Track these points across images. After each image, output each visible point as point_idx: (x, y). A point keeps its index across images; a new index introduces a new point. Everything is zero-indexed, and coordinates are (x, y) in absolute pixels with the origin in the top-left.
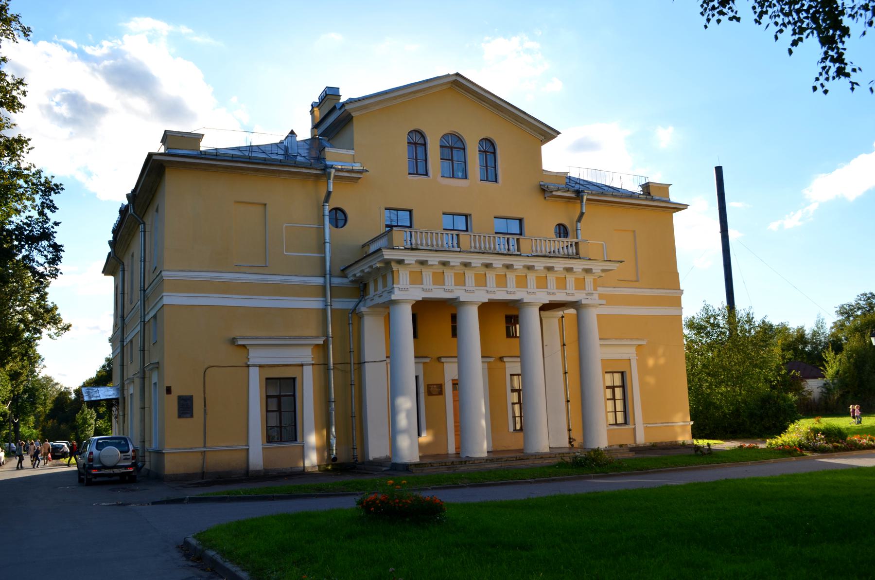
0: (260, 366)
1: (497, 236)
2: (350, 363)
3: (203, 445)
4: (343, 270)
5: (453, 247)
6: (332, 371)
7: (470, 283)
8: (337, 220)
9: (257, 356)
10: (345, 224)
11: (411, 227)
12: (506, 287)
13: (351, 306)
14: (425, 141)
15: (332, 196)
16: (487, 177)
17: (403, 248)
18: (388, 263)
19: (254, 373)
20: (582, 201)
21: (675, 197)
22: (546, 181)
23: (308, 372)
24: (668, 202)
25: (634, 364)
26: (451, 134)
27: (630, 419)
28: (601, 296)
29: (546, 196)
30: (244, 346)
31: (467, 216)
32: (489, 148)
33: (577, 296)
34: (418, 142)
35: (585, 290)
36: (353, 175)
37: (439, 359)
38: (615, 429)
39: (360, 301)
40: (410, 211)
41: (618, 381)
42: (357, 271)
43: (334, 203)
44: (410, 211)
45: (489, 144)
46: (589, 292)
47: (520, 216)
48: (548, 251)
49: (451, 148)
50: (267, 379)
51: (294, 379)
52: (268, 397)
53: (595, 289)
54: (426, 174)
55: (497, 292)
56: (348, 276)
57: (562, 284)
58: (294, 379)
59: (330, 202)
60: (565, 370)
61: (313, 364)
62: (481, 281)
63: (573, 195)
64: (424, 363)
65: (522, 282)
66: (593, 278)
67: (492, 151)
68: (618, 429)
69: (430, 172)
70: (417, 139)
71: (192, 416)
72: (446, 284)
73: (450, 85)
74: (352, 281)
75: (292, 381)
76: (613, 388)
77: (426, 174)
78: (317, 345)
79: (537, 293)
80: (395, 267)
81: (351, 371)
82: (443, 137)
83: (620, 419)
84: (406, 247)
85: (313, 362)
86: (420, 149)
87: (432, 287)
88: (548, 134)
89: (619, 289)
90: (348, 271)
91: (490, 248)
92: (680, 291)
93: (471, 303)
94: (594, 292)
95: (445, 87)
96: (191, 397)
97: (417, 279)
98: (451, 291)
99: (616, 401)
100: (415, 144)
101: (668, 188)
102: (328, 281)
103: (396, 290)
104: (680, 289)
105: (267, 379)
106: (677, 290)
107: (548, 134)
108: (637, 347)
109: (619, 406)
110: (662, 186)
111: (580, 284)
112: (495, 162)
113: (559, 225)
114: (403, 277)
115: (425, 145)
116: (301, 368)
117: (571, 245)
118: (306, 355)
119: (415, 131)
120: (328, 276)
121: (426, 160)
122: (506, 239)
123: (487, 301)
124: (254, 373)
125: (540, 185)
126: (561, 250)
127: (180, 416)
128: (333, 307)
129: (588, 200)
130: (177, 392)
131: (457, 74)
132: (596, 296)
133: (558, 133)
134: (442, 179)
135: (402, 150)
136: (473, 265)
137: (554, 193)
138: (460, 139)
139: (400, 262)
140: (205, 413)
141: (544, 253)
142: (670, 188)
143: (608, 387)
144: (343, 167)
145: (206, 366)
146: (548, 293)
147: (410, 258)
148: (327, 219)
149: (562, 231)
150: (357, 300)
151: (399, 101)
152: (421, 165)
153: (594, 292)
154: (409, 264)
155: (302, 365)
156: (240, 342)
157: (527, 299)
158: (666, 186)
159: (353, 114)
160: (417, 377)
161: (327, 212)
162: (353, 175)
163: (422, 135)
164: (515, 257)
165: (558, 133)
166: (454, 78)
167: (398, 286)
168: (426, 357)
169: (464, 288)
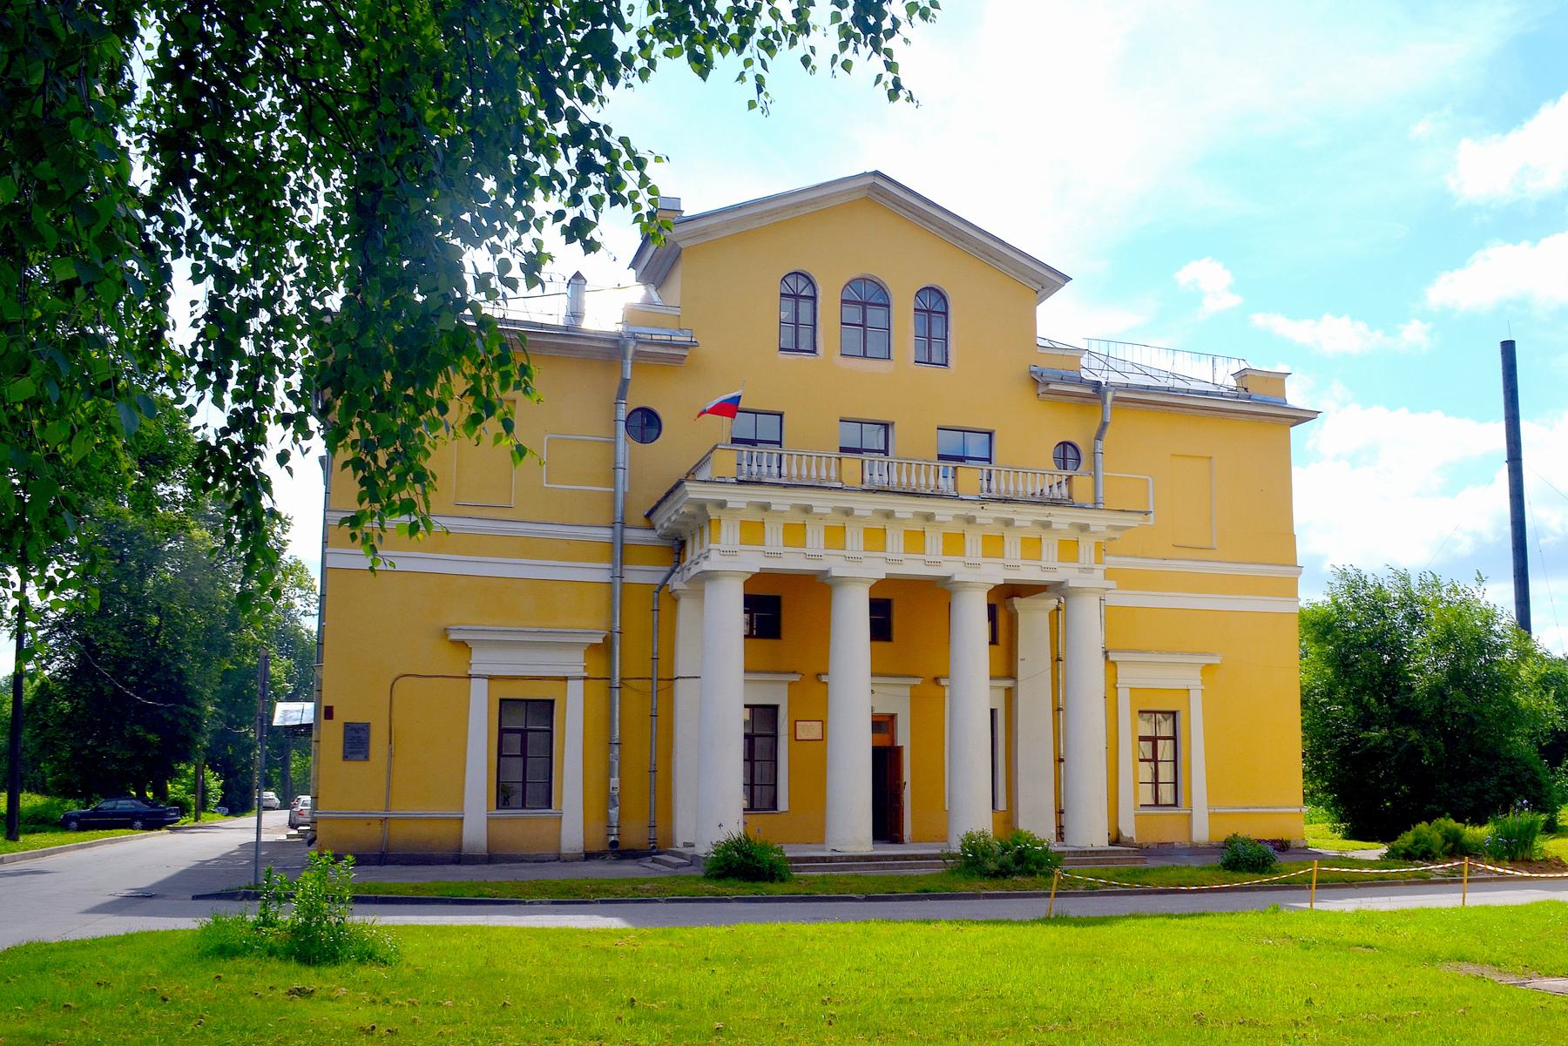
0: (490, 678)
1: (942, 464)
2: (658, 679)
3: (384, 808)
4: (648, 516)
5: (780, 476)
6: (617, 691)
7: (1087, 558)
8: (1065, 459)
9: (483, 661)
10: (657, 437)
11: (989, 460)
12: (885, 551)
13: (657, 579)
14: (815, 291)
15: (630, 387)
16: (930, 357)
17: (734, 480)
18: (702, 506)
19: (479, 689)
20: (1104, 402)
21: (1295, 396)
22: (1044, 364)
23: (575, 691)
24: (1282, 404)
25: (1196, 700)
26: (864, 279)
27: (1182, 799)
28: (1108, 575)
29: (1040, 391)
30: (463, 643)
31: (886, 426)
32: (933, 306)
33: (1065, 573)
34: (804, 294)
35: (1077, 562)
36: (672, 351)
37: (936, 679)
38: (1152, 815)
39: (673, 571)
40: (781, 415)
41: (1166, 729)
42: (665, 519)
43: (636, 399)
44: (781, 415)
45: (802, 283)
46: (1085, 566)
47: (988, 427)
48: (1030, 491)
49: (929, 311)
50: (502, 701)
51: (552, 702)
52: (502, 731)
53: (1099, 561)
54: (814, 351)
55: (864, 560)
56: (657, 527)
57: (1032, 548)
58: (552, 702)
59: (628, 397)
60: (1058, 704)
61: (585, 678)
62: (993, 545)
63: (1089, 391)
64: (791, 683)
65: (954, 543)
66: (783, 522)
67: (810, 294)
68: (1157, 815)
69: (820, 350)
70: (930, 301)
71: (367, 758)
72: (889, 549)
73: (866, 192)
74: (662, 537)
75: (546, 708)
76: (1154, 740)
77: (814, 351)
78: (594, 646)
79: (982, 565)
80: (713, 513)
81: (652, 692)
82: (848, 284)
83: (1166, 794)
84: (741, 478)
85: (586, 674)
86: (805, 307)
87: (782, 550)
88: (1045, 280)
89: (1174, 562)
90: (655, 517)
91: (927, 486)
92: (1296, 569)
93: (855, 580)
94: (1095, 566)
95: (856, 196)
96: (368, 725)
97: (753, 532)
98: (819, 558)
99: (1160, 764)
100: (796, 297)
101: (1283, 381)
102: (619, 533)
103: (714, 555)
104: (1296, 566)
105: (502, 701)
106: (1289, 566)
107: (1045, 280)
108: (588, 648)
109: (1166, 772)
110: (1271, 376)
111: (1069, 550)
112: (947, 330)
113: (1064, 444)
114: (728, 534)
115: (814, 298)
116: (563, 683)
117: (1059, 484)
118: (573, 663)
119: (930, 289)
120: (618, 526)
121: (815, 326)
122: (985, 471)
123: (758, 571)
124: (479, 689)
125: (1031, 372)
126: (1047, 491)
127: (345, 758)
128: (624, 580)
129: (1115, 399)
130: (341, 717)
131: (877, 174)
132: (1099, 574)
133: (1067, 279)
134: (843, 358)
135: (769, 311)
136: (1092, 529)
137: (1052, 387)
138: (881, 289)
139: (722, 505)
140: (391, 755)
141: (1003, 495)
142: (1288, 380)
143: (1142, 739)
144: (654, 337)
145: (396, 674)
146: (1007, 567)
147: (739, 498)
148: (622, 425)
149: (1067, 454)
150: (668, 569)
151: (766, 221)
152: (805, 334)
153: (1095, 566)
154: (944, 522)
155: (566, 679)
156: (454, 636)
157: (836, 565)
158: (1280, 377)
159: (682, 245)
160: (993, 711)
161: (622, 415)
162: (672, 351)
163: (942, 296)
164: (768, 488)
165: (1067, 279)
166: (870, 180)
167: (717, 546)
168: (794, 672)
169: (883, 555)
